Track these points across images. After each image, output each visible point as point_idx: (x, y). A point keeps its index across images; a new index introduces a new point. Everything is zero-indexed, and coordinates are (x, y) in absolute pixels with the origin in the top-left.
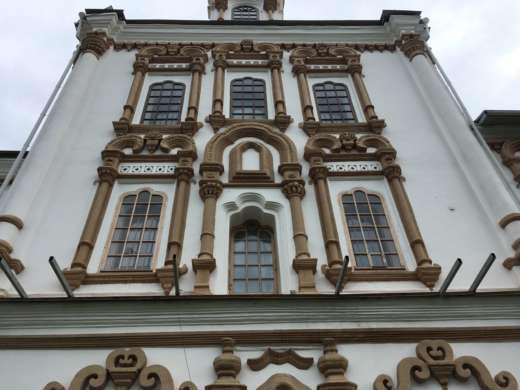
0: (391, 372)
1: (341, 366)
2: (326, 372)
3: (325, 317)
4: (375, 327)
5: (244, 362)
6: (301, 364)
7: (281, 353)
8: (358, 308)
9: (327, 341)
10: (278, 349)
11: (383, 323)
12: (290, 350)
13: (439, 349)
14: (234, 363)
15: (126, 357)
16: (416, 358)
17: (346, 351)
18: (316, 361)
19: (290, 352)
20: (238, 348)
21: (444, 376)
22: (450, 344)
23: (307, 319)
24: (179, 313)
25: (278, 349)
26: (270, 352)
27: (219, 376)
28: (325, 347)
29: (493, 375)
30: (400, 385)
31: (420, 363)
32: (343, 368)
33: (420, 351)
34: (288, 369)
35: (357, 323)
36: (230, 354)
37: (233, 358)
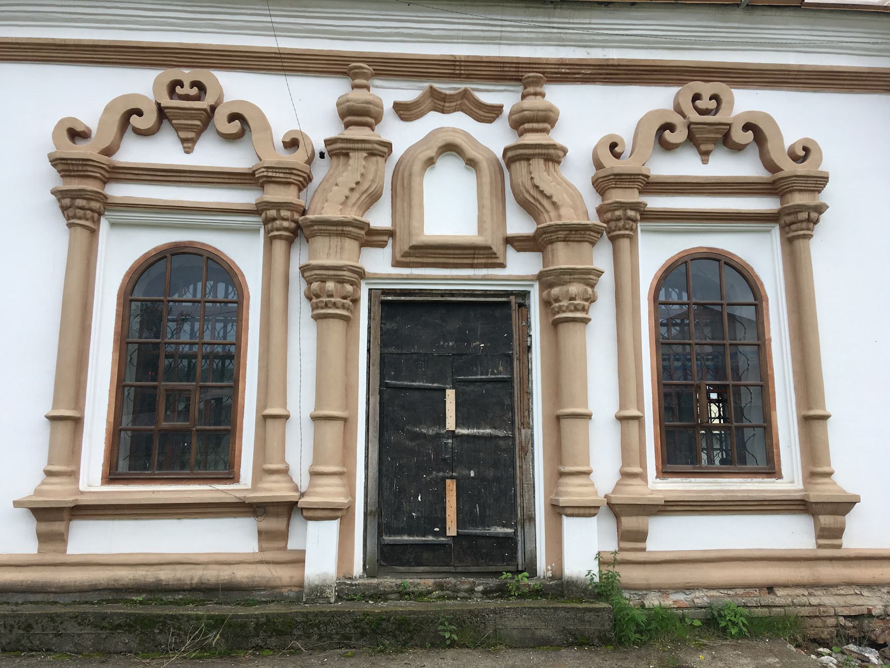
0: (625, 133)
1: (546, 119)
2: (522, 127)
3: (533, 35)
4: (615, 57)
5: (388, 106)
6: (482, 113)
7: (450, 95)
8: (593, 21)
9: (529, 77)
10: (445, 87)
11: (631, 50)
12: (466, 90)
13: (715, 97)
14: (371, 106)
15: (187, 84)
16: (670, 111)
17: (558, 96)
18: (506, 110)
19: (465, 94)
20: (377, 82)
21: (708, 141)
22: (734, 91)
23: (501, 38)
24: (272, 13)
25: (445, 87)
26: (433, 93)
27: (347, 125)
28: (525, 88)
29: (788, 143)
30: (636, 150)
31: (677, 119)
32: (549, 123)
33: (681, 101)
34: (459, 122)
35: (585, 49)
36: (365, 91)
37: (370, 98)
